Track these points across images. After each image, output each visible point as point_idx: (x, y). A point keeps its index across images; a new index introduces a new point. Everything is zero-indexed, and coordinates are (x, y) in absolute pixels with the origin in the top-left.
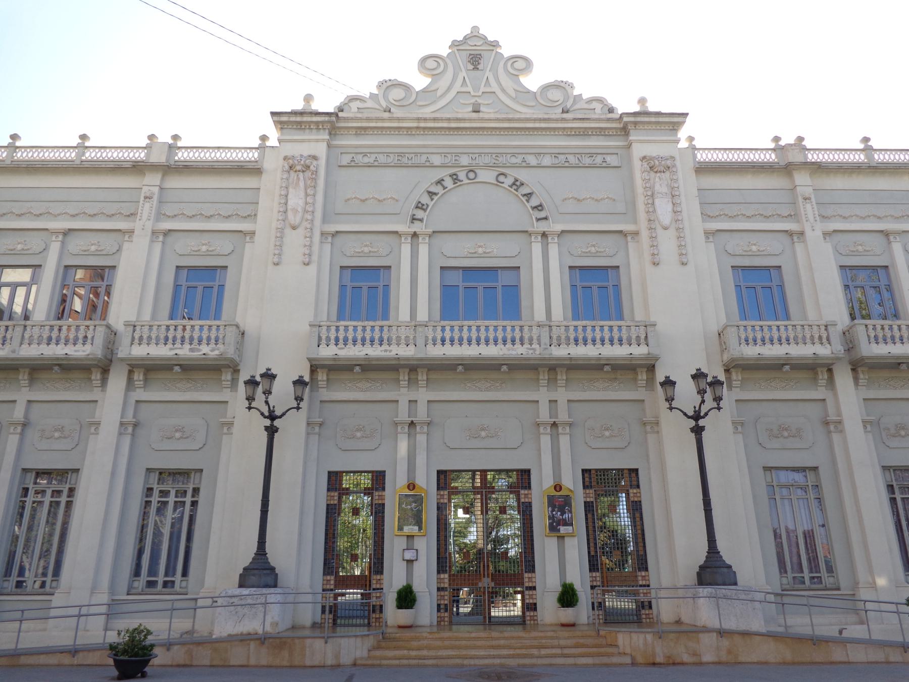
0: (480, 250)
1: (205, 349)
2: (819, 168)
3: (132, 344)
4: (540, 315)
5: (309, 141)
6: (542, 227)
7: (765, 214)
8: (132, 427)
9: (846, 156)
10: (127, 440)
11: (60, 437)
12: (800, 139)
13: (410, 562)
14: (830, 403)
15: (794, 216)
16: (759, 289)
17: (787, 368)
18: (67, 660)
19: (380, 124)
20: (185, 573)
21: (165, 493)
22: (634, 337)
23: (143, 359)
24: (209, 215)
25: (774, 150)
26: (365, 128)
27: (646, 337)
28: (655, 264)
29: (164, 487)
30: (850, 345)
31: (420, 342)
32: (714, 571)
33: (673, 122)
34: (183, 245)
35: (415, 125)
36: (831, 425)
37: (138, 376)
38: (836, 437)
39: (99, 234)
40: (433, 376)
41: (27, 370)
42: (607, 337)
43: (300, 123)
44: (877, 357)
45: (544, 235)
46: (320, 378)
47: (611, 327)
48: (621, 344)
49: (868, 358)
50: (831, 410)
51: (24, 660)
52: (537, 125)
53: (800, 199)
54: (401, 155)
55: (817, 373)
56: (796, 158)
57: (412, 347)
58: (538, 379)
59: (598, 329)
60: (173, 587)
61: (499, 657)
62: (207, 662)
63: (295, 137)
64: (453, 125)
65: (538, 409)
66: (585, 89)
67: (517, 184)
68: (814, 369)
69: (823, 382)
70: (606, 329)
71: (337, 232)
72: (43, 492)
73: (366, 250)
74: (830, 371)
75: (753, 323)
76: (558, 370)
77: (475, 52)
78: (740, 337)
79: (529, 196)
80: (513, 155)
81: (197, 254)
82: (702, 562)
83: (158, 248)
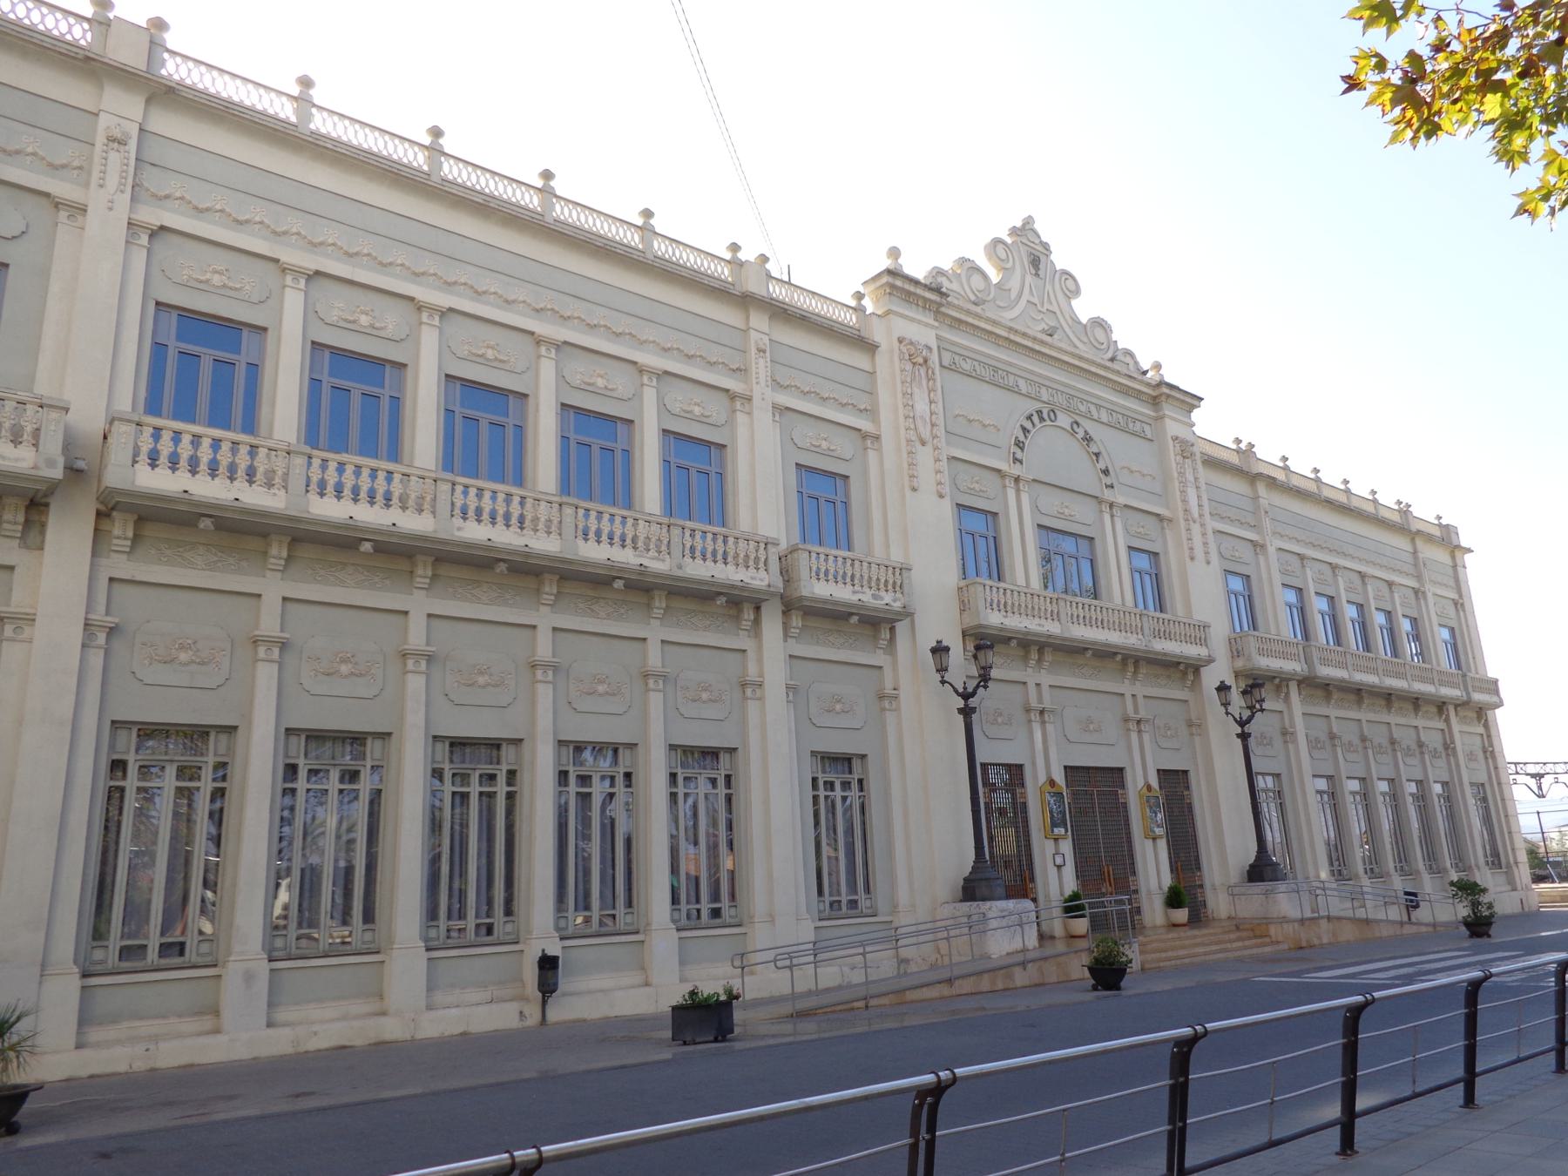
0: (824, 445)
1: (888, 598)
2: (169, 95)
3: (135, 462)
4: (1021, 581)
5: (919, 322)
6: (1016, 470)
7: (195, 202)
8: (103, 634)
9: (518, 193)
10: (96, 660)
11: (352, 674)
12: (159, 25)
13: (1059, 867)
14: (888, 672)
15: (741, 371)
16: (693, 472)
17: (503, 567)
18: (945, 990)
19: (976, 322)
20: (867, 890)
21: (463, 778)
22: (29, 429)
23: (825, 601)
24: (57, 162)
25: (854, 309)
26: (960, 321)
27: (286, 474)
28: (914, 489)
29: (689, 772)
30: (787, 573)
31: (568, 530)
32: (1261, 870)
33: (1190, 401)
34: (806, 434)
35: (1004, 334)
36: (748, 687)
37: (121, 529)
38: (1291, 746)
39: (704, 390)
40: (444, 570)
41: (131, 518)
42: (364, 489)
43: (909, 293)
44: (586, 563)
45: (1017, 480)
46: (117, 531)
47: (374, 471)
48: (213, 476)
49: (806, 598)
50: (752, 670)
51: (911, 996)
52: (1093, 369)
53: (754, 350)
54: (995, 370)
55: (740, 611)
56: (753, 286)
57: (427, 515)
58: (265, 554)
59: (365, 473)
60: (182, 953)
61: (1177, 958)
62: (1054, 979)
63: (907, 313)
64: (1037, 347)
65: (406, 630)
66: (1123, 338)
67: (1088, 439)
68: (737, 604)
69: (746, 624)
70: (186, 439)
71: (162, 228)
72: (492, 778)
73: (217, 280)
74: (758, 609)
75: (828, 551)
76: (420, 558)
77: (1027, 250)
78: (308, 479)
79: (1024, 430)
80: (965, 358)
81: (350, 327)
82: (1252, 861)
83: (139, 258)
